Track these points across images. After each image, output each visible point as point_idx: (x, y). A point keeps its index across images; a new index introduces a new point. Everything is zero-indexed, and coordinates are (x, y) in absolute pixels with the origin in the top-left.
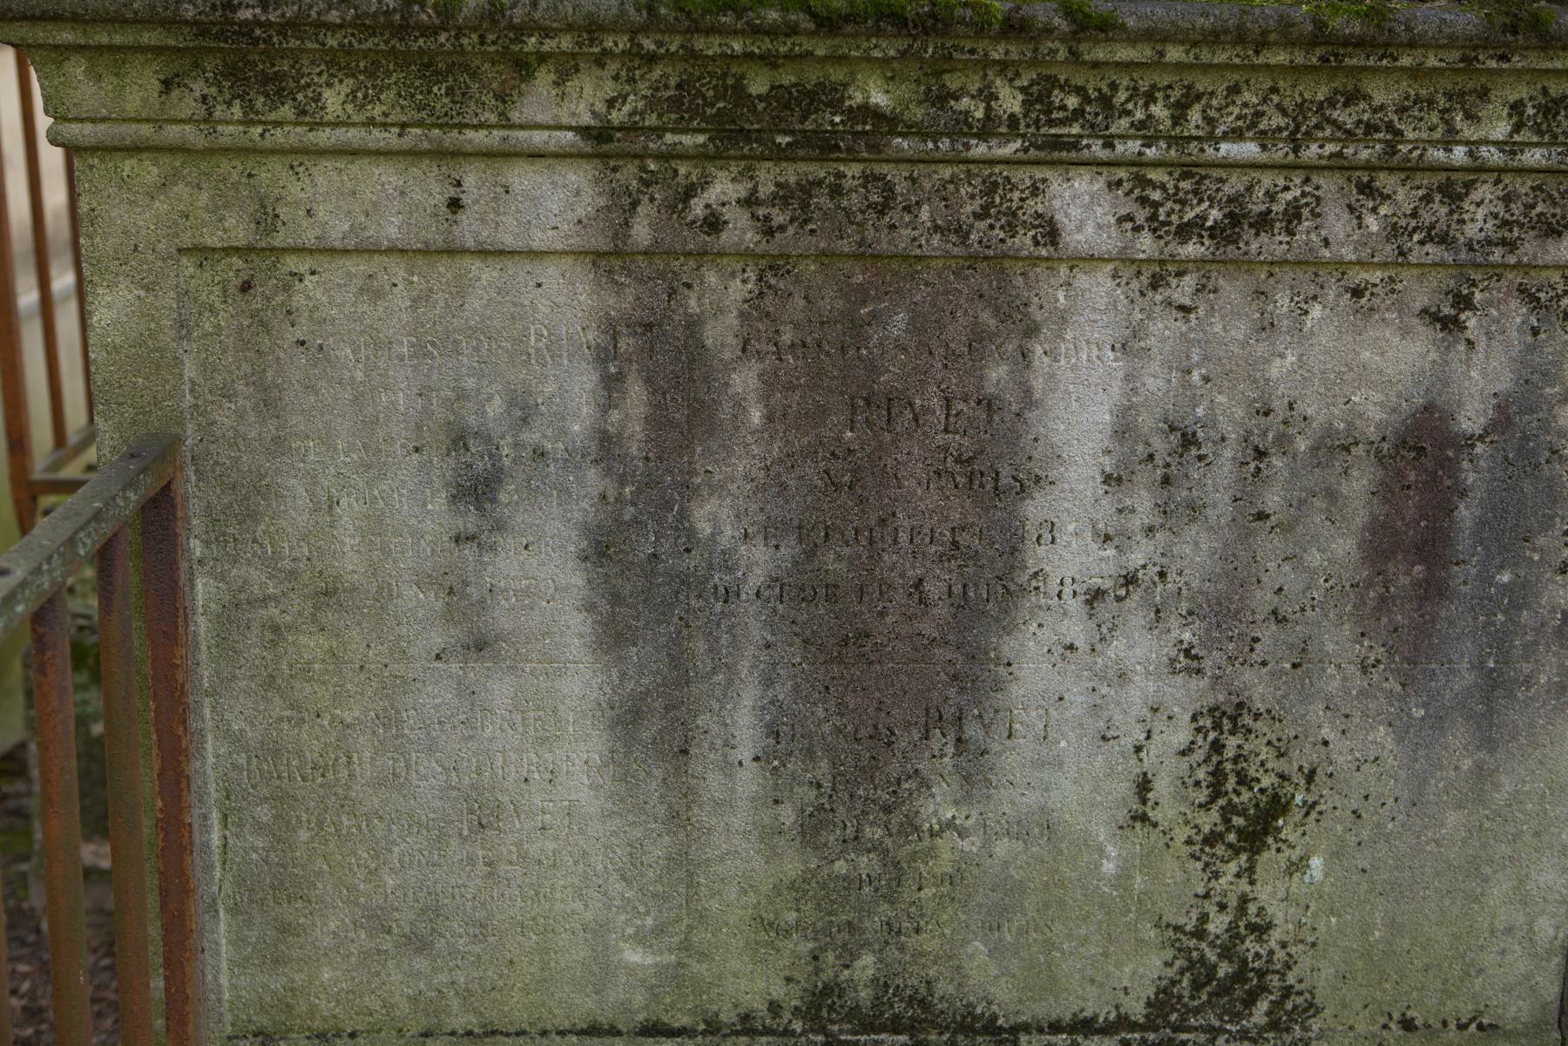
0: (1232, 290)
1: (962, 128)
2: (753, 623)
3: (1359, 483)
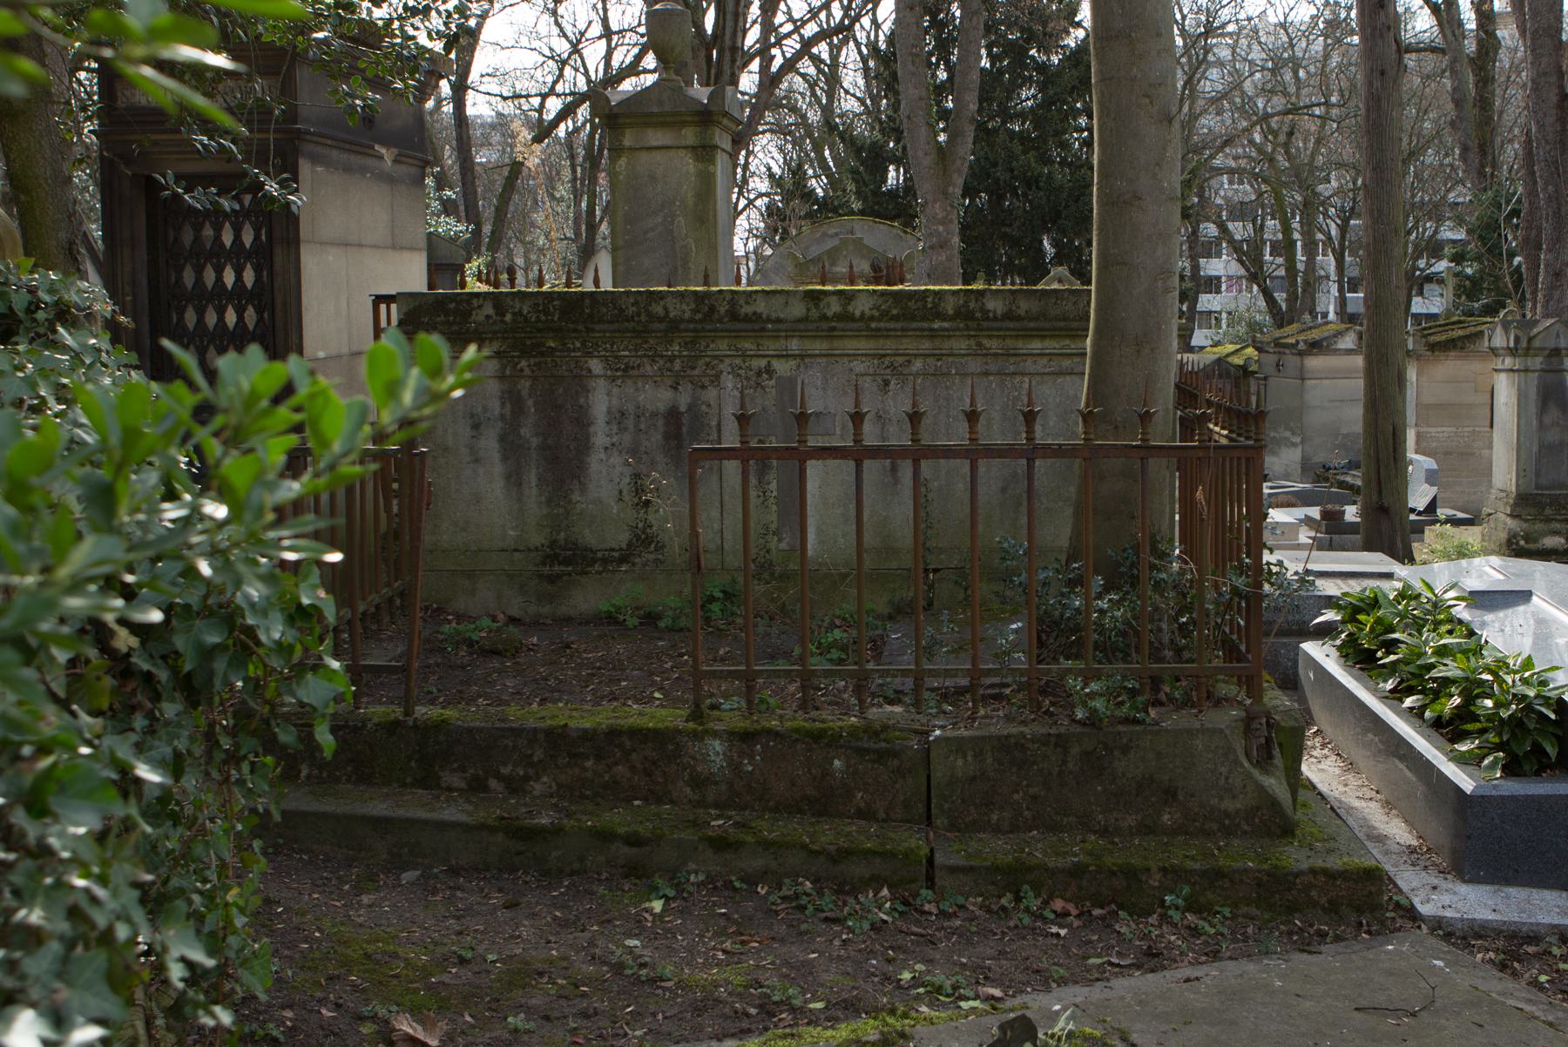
0: (629, 382)
1: (569, 350)
3: (660, 423)
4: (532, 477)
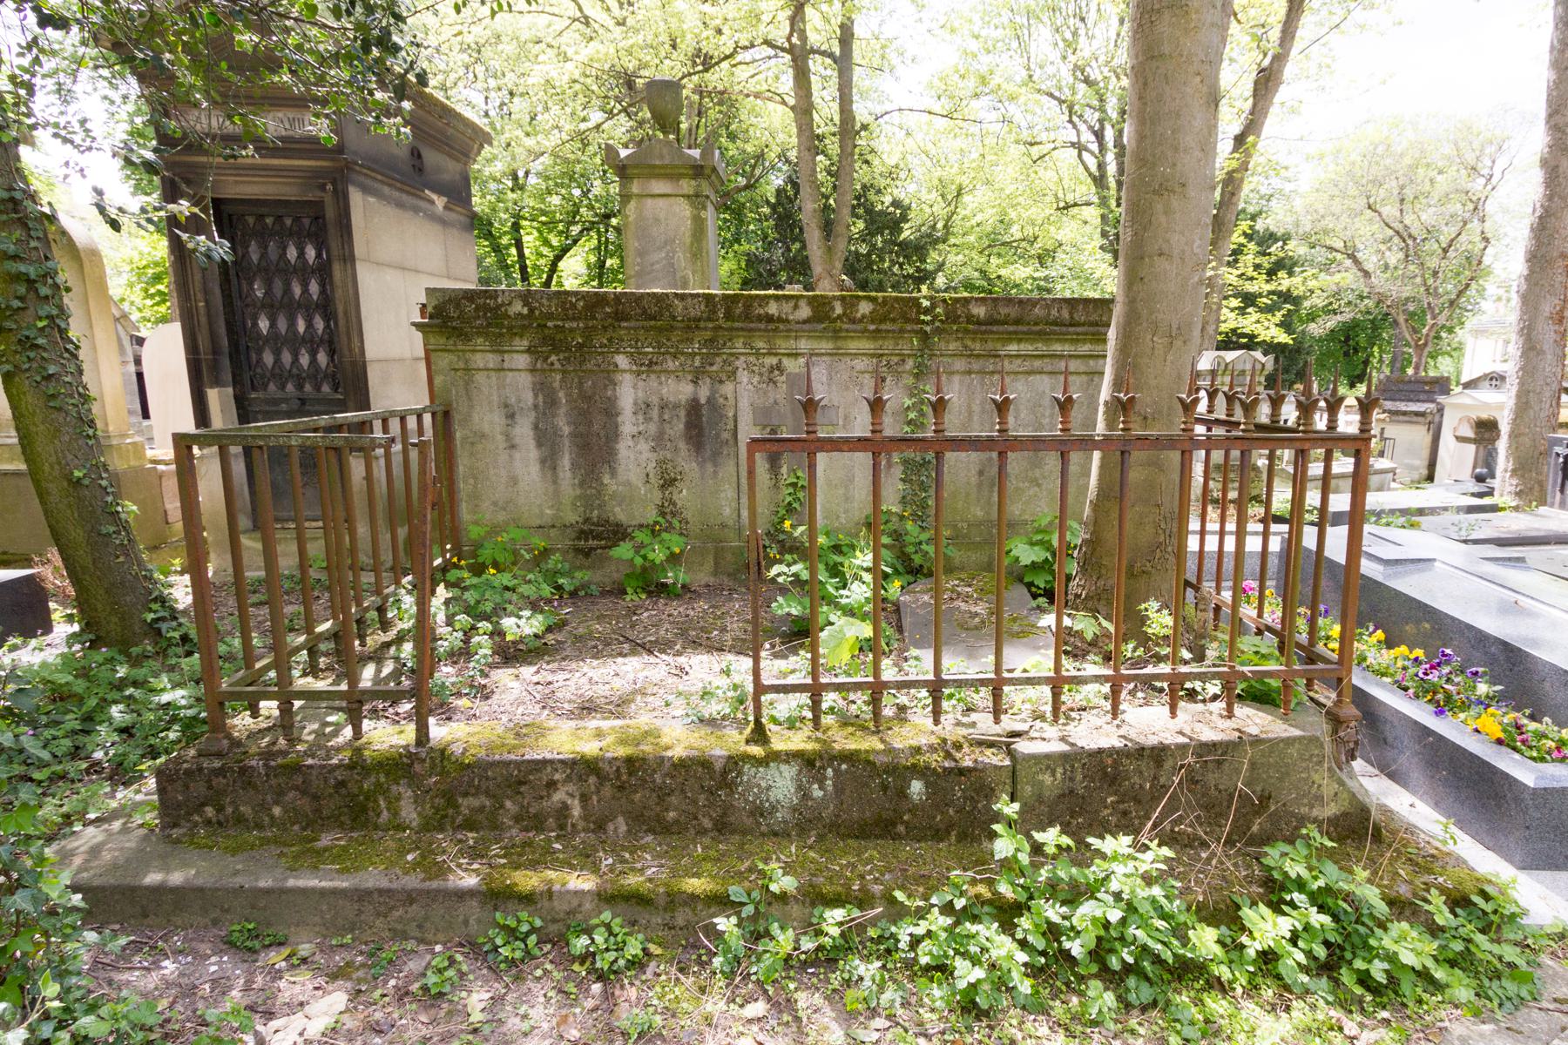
0: (653, 376)
2: (567, 442)
3: (683, 413)
4: (566, 462)
